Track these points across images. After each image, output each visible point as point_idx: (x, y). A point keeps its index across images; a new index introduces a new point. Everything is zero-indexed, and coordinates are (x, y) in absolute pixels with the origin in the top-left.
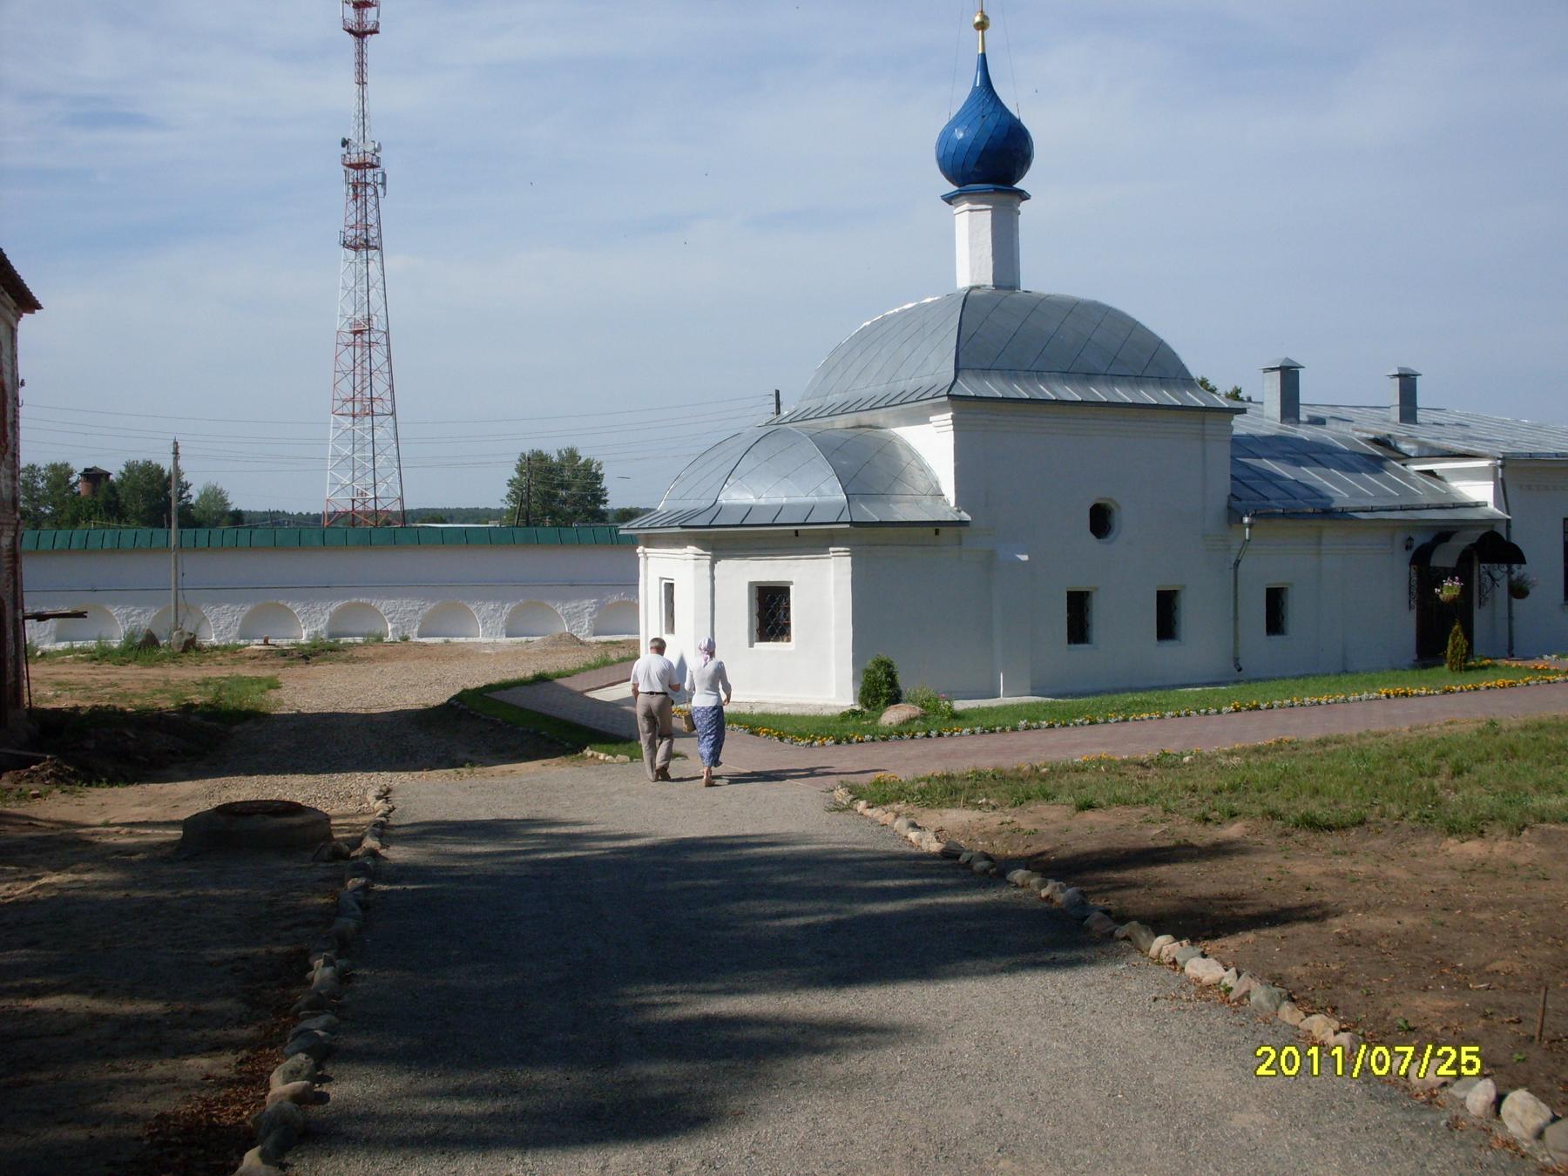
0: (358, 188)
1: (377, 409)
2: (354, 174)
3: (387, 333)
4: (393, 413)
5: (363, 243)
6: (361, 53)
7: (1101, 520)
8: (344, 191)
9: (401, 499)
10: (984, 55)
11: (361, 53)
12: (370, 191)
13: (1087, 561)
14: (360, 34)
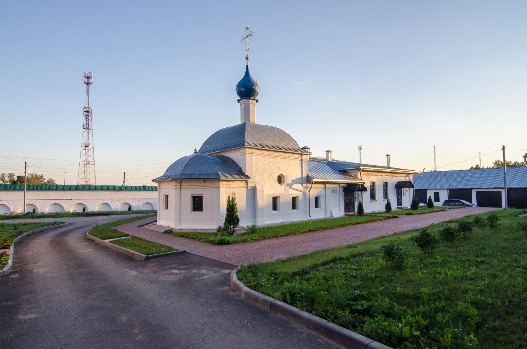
0: (86, 117)
1: (90, 163)
2: (86, 113)
3: (93, 147)
4: (94, 164)
5: (87, 128)
6: (88, 88)
7: (280, 180)
8: (83, 117)
9: (95, 182)
10: (247, 66)
11: (88, 88)
12: (90, 117)
13: (279, 190)
14: (88, 84)
